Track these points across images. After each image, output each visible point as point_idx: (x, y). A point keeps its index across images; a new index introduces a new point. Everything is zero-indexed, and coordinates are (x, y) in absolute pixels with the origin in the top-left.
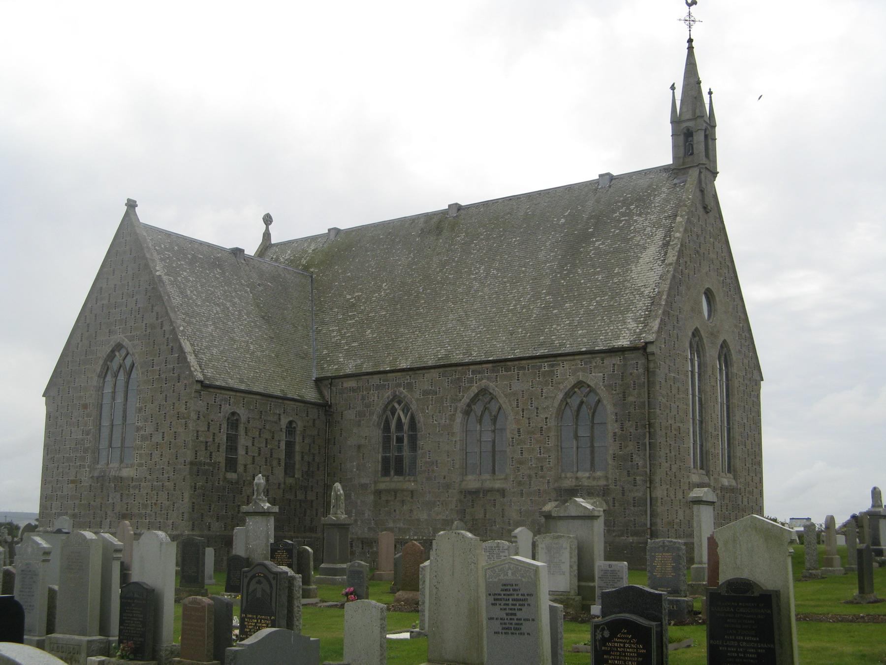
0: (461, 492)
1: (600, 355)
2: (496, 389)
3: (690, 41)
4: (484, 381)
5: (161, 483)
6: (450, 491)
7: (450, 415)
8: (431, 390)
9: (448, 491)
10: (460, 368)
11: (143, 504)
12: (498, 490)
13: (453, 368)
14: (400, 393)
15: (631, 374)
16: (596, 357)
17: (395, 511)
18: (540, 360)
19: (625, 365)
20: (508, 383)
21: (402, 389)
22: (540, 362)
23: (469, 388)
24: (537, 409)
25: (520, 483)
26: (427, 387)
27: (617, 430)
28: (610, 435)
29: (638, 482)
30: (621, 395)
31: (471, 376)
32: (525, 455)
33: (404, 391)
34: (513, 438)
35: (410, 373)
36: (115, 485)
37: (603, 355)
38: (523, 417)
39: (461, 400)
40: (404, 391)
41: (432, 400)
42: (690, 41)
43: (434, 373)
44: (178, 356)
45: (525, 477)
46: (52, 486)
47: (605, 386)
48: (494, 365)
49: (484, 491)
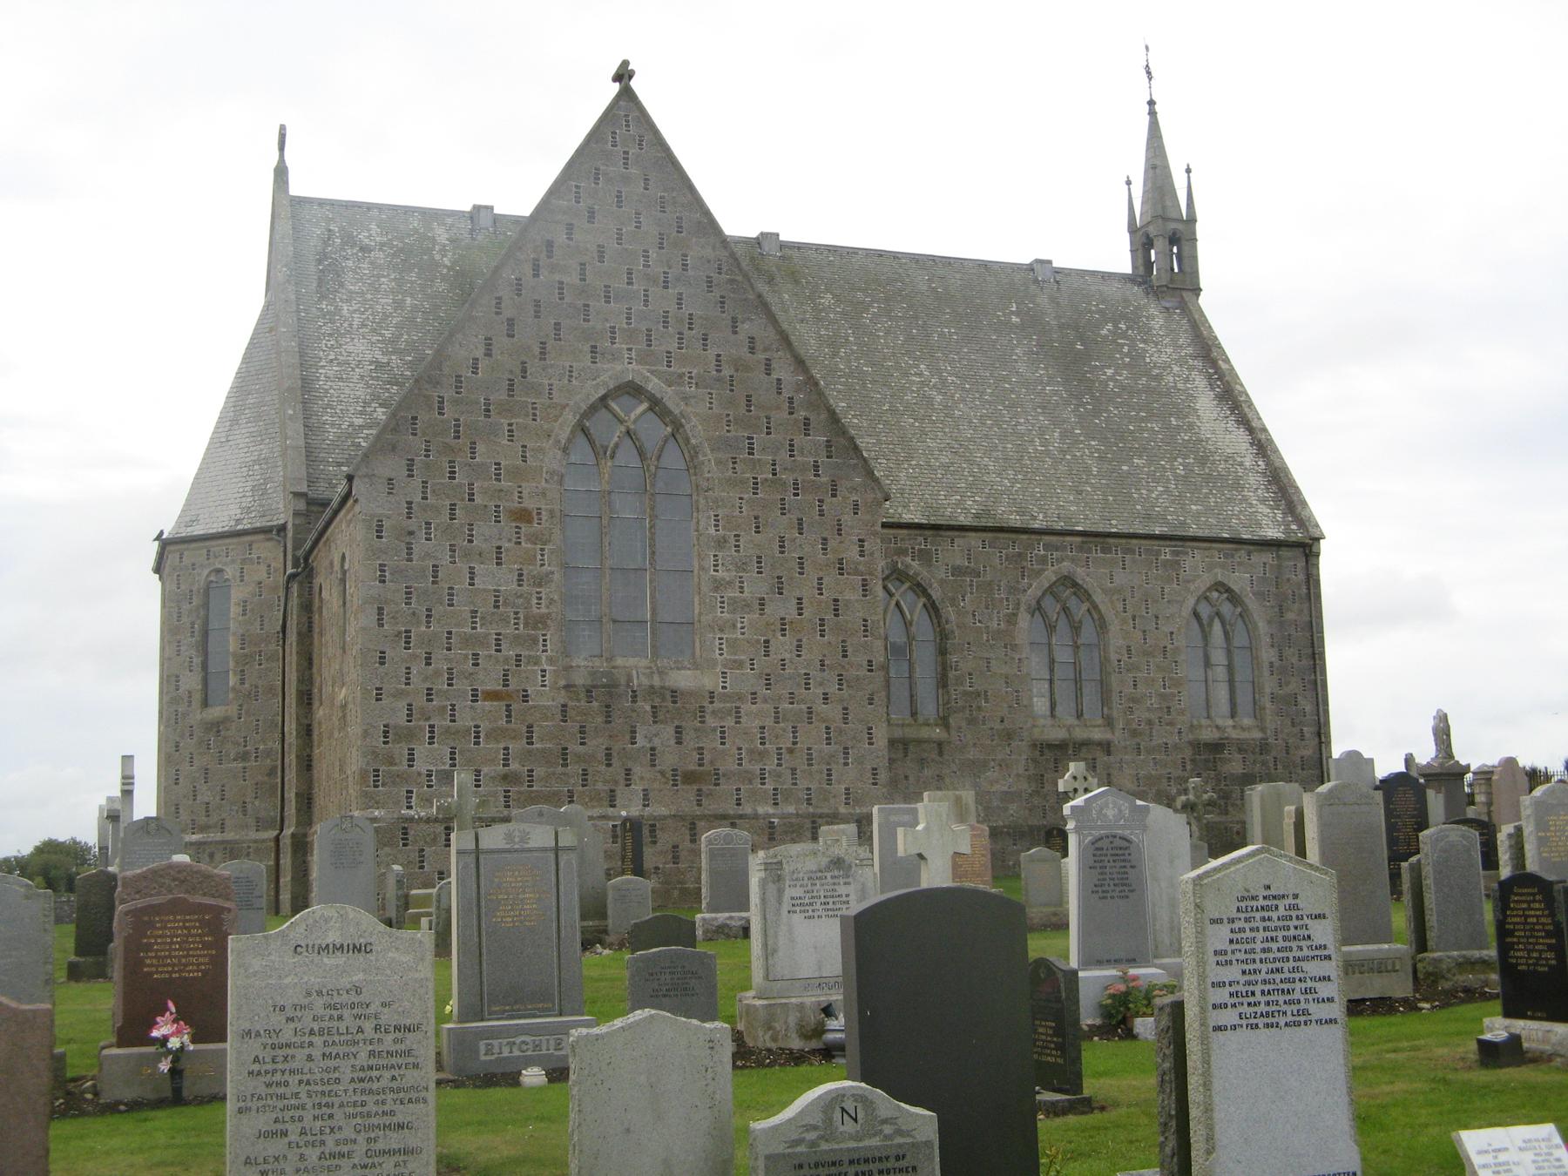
0: (1034, 745)
1: (1245, 547)
2: (1088, 579)
3: (1151, 103)
4: (1065, 563)
5: (804, 707)
6: (1014, 744)
7: (1007, 615)
8: (968, 567)
9: (1009, 744)
10: (1025, 537)
11: (751, 752)
12: (1100, 744)
13: (1013, 536)
14: (907, 566)
15: (1288, 580)
16: (1240, 549)
17: (906, 777)
18: (1162, 543)
19: (1279, 566)
20: (1107, 571)
21: (909, 559)
22: (1159, 546)
23: (1039, 573)
24: (1157, 617)
25: (1135, 733)
26: (961, 561)
27: (1273, 659)
28: (1266, 665)
29: (1307, 735)
30: (1277, 610)
31: (1042, 552)
32: (1142, 689)
33: (913, 563)
34: (1119, 661)
35: (928, 533)
36: (653, 707)
37: (1251, 548)
38: (1134, 628)
39: (1025, 591)
40: (913, 563)
41: (971, 585)
42: (1151, 103)
43: (974, 540)
44: (827, 441)
45: (1143, 724)
46: (410, 705)
47: (1254, 594)
48: (1085, 539)
49: (1075, 744)
